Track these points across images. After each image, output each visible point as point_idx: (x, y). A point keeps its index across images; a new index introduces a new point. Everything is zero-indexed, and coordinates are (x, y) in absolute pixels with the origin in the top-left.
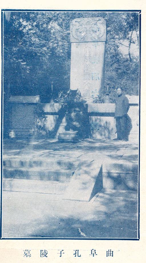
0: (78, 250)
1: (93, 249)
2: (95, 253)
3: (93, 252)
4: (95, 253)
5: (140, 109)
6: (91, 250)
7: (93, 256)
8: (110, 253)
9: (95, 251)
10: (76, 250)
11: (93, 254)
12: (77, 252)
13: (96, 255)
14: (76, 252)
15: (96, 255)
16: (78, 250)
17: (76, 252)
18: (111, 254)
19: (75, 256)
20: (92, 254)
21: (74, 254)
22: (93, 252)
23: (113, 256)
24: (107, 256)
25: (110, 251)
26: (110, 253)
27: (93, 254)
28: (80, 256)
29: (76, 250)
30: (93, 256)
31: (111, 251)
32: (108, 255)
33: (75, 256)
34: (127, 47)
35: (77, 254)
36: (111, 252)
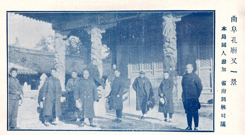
0: (235, 37)
1: (234, 26)
2: (236, 30)
3: (234, 29)
4: (236, 30)
5: (54, 130)
6: (233, 27)
7: (234, 32)
8: (234, 19)
9: (235, 27)
10: (234, 38)
11: (233, 30)
12: (234, 39)
13: (237, 31)
14: (233, 39)
15: (237, 31)
16: (235, 37)
17: (233, 39)
18: (235, 20)
19: (233, 42)
20: (233, 30)
21: (232, 41)
22: (234, 29)
23: (236, 22)
24: (232, 22)
25: (234, 17)
26: (234, 19)
27: (234, 30)
28: (237, 43)
29: (234, 38)
30: (234, 32)
31: (235, 17)
32: (232, 20)
33: (233, 42)
34: (88, 125)
35: (234, 41)
36: (235, 18)
